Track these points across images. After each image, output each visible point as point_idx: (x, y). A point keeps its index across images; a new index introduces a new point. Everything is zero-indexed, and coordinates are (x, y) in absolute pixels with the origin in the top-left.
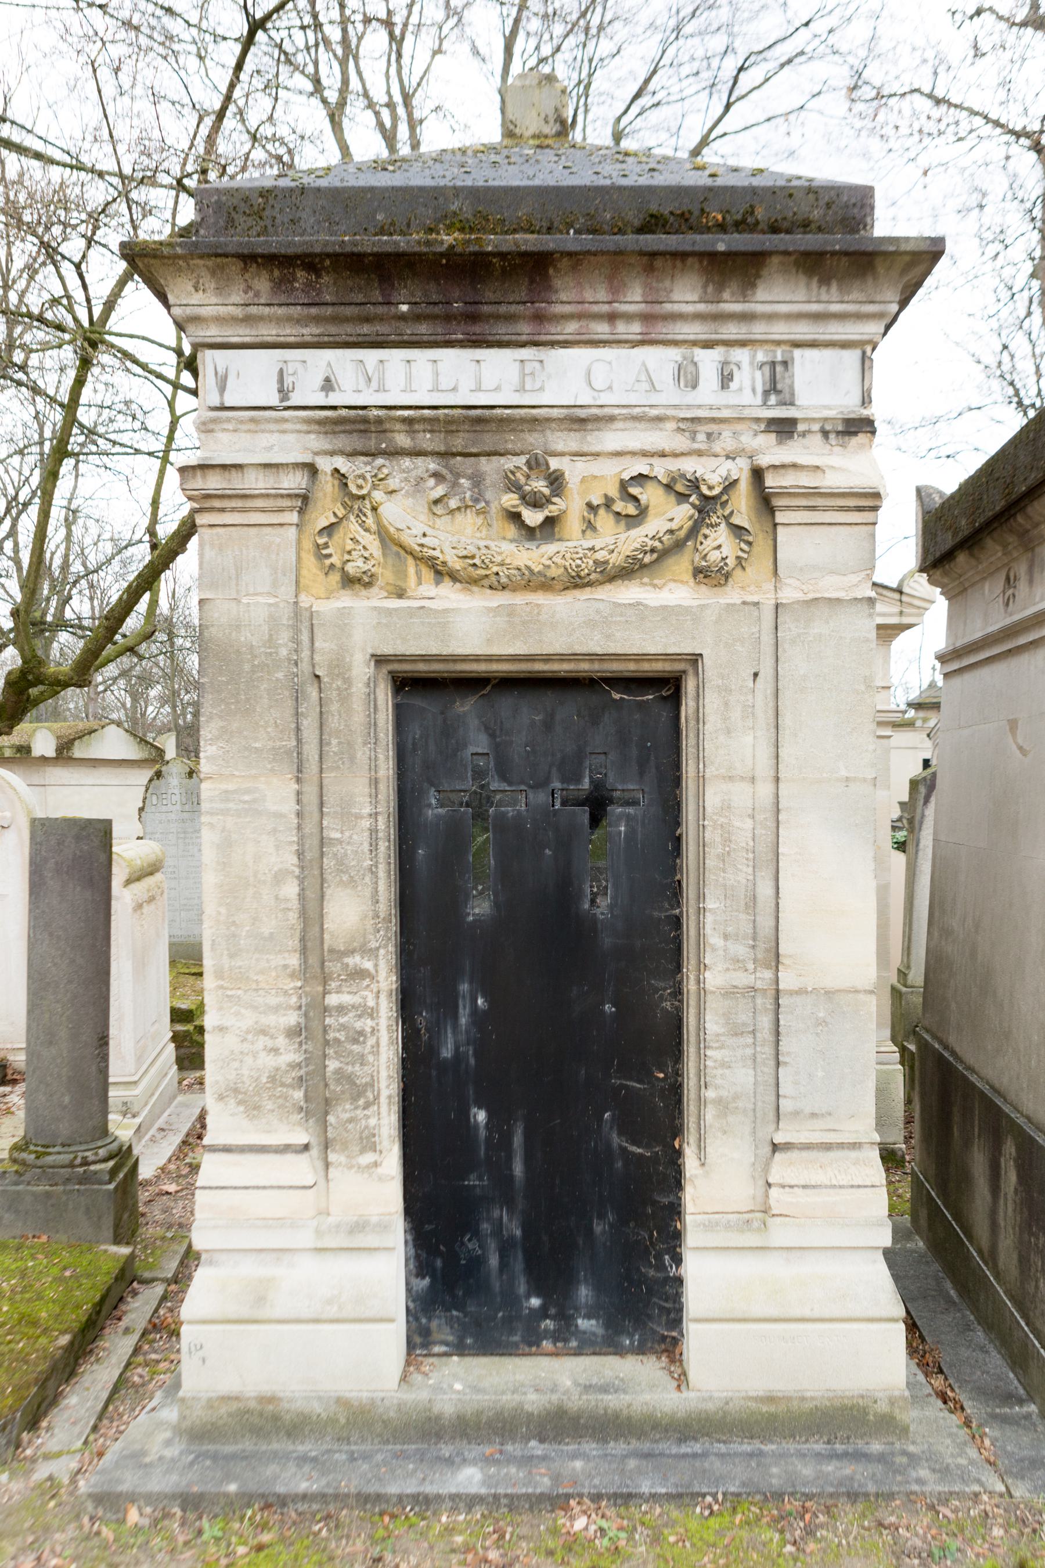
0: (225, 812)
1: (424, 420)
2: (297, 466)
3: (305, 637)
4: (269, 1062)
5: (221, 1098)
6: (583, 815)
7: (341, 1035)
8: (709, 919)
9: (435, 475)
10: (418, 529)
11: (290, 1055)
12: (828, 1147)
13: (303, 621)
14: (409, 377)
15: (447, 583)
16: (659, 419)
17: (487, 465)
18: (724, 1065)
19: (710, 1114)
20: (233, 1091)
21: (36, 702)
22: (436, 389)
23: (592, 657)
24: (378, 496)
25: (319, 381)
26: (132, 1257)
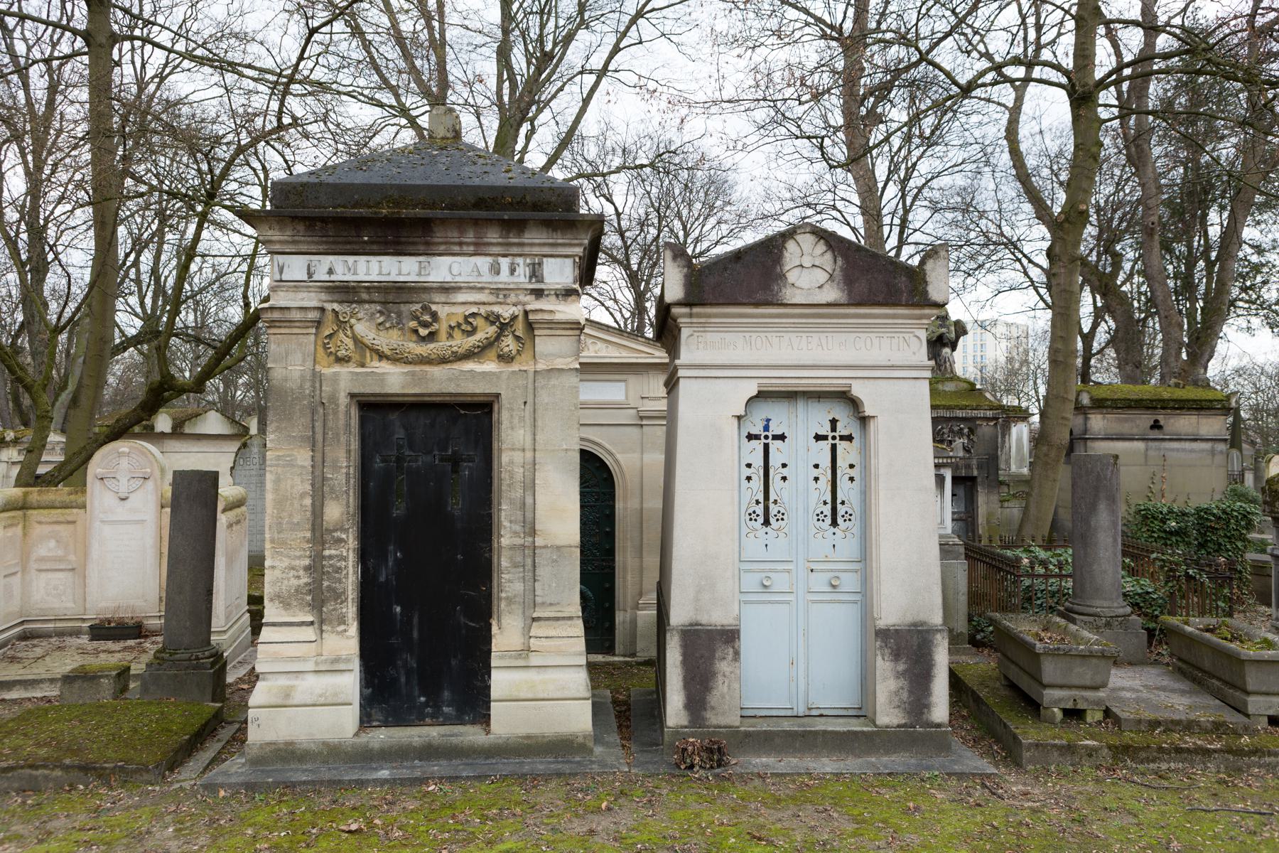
0: (277, 466)
1: (374, 287)
2: (315, 308)
3: (317, 385)
4: (295, 582)
5: (271, 600)
6: (448, 466)
7: (330, 570)
8: (503, 514)
9: (380, 312)
10: (372, 335)
11: (305, 580)
12: (557, 619)
13: (316, 377)
14: (368, 269)
15: (385, 361)
16: (482, 288)
17: (404, 308)
18: (510, 581)
19: (503, 605)
20: (278, 597)
21: (168, 400)
22: (380, 274)
23: (451, 394)
24: (353, 321)
25: (326, 269)
26: (222, 708)
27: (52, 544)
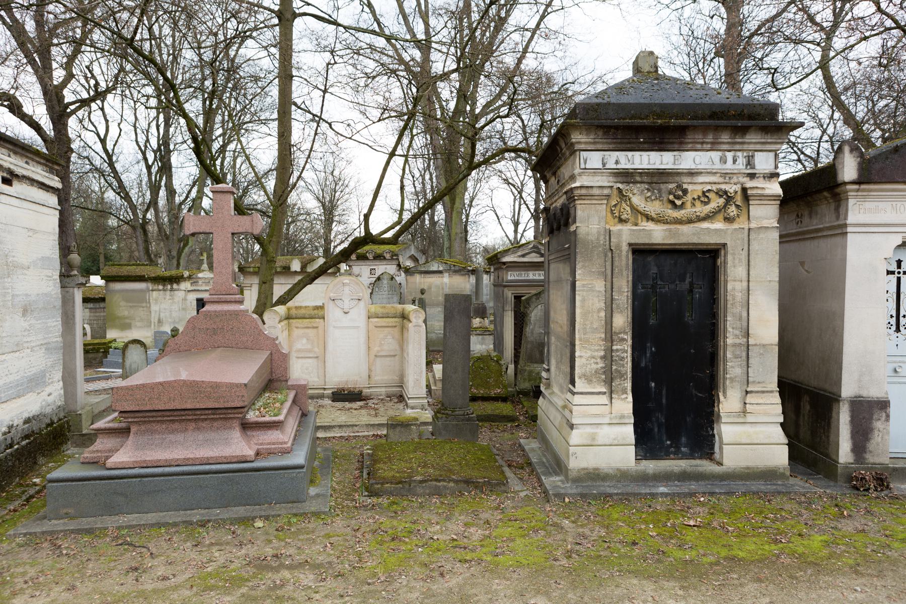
0: (583, 291)
4: (594, 366)
5: (580, 378)
9: (648, 190)
10: (643, 206)
11: (601, 365)
12: (763, 392)
17: (663, 186)
18: (732, 367)
19: (728, 382)
20: (584, 376)
27: (304, 341)
